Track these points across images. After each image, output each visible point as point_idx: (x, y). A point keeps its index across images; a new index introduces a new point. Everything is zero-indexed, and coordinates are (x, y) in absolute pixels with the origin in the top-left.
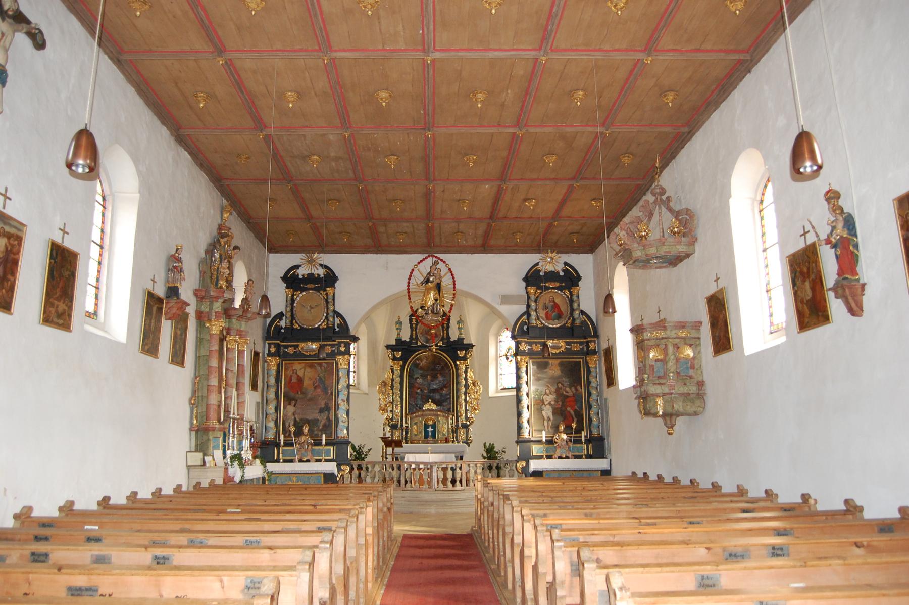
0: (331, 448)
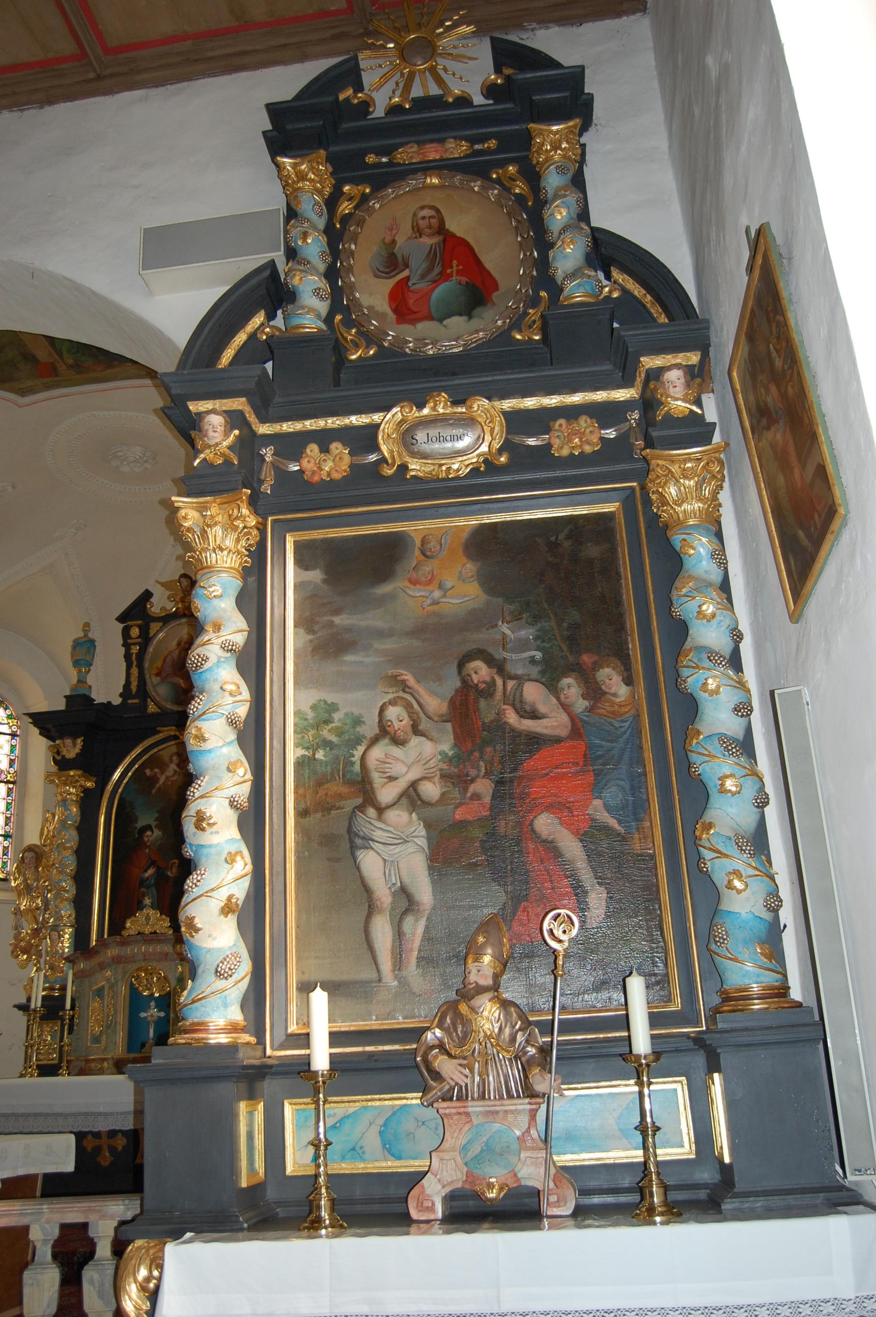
0: (704, 1028)
